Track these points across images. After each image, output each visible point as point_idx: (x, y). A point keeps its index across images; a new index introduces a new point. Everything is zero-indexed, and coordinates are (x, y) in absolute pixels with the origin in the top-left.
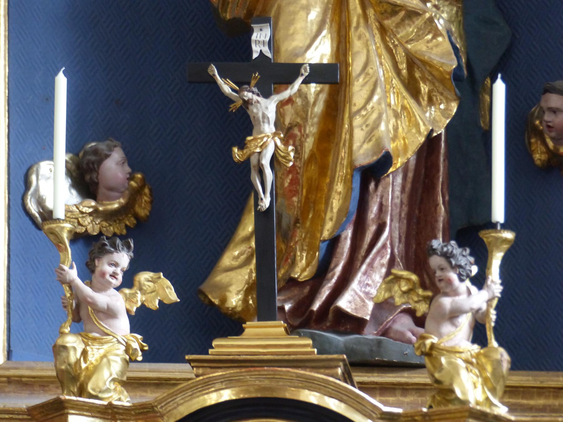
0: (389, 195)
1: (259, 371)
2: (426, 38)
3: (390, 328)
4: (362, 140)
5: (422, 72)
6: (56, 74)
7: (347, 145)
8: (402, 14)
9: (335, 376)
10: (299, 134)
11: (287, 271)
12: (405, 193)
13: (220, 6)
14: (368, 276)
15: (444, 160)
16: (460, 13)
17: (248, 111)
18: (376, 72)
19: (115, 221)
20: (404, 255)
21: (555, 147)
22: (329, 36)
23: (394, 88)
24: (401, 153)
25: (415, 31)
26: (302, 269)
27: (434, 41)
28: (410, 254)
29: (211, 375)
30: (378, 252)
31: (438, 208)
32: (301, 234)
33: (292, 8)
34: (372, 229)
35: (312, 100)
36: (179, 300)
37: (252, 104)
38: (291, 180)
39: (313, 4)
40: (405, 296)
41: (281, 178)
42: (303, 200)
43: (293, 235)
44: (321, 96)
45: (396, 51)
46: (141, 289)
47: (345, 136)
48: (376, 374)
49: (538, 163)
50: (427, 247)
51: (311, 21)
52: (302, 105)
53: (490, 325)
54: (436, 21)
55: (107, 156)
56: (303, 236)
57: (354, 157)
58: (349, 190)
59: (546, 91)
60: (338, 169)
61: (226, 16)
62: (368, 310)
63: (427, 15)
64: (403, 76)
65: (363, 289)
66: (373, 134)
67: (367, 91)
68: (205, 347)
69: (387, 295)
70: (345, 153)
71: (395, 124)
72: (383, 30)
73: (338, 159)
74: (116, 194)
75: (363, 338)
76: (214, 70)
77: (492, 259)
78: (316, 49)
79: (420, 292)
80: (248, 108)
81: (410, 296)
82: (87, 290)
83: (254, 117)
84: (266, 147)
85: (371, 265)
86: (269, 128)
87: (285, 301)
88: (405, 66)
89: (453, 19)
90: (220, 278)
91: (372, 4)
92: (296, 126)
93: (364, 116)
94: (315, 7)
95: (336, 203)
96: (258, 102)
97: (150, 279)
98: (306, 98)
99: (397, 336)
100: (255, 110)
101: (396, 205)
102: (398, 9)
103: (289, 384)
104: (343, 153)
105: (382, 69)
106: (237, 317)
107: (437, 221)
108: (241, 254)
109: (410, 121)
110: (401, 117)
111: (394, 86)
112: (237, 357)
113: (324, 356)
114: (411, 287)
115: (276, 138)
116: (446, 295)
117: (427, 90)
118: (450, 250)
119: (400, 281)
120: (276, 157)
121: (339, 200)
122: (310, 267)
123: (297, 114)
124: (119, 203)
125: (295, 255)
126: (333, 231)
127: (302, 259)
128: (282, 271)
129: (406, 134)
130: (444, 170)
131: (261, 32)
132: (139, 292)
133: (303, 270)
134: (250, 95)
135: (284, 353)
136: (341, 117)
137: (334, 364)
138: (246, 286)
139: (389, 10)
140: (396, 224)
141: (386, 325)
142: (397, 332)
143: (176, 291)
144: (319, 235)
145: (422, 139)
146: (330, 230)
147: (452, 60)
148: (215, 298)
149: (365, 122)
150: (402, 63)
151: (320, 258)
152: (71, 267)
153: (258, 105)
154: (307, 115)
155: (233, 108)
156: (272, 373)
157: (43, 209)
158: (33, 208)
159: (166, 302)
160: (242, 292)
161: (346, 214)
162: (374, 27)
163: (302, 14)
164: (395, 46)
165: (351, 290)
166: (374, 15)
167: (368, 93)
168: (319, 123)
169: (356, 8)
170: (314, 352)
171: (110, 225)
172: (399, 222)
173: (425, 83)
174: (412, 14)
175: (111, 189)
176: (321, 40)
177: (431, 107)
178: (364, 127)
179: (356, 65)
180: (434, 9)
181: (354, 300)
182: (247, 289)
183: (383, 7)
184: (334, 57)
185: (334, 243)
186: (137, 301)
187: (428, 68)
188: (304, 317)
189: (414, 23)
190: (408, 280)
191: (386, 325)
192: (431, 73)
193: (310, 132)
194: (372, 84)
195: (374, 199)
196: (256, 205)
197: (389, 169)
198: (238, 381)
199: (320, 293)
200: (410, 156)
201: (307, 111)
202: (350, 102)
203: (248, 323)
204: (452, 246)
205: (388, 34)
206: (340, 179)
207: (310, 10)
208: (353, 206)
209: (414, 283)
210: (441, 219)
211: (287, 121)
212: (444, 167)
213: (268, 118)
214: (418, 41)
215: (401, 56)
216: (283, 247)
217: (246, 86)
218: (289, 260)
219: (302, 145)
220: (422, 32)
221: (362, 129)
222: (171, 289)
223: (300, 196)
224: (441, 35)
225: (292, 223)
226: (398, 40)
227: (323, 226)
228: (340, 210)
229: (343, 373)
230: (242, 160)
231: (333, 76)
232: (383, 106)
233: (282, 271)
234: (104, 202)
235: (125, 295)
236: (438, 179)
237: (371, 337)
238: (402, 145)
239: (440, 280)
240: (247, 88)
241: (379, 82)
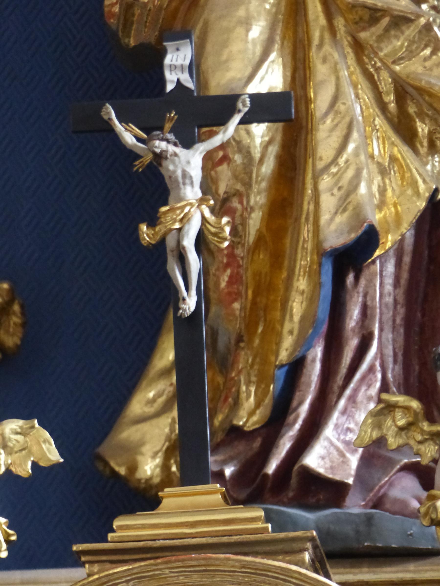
0: (375, 290)
1: (183, 561)
2: (422, 54)
3: (385, 495)
4: (333, 211)
5: (418, 105)
7: (311, 219)
8: (386, 21)
9: (301, 564)
10: (239, 207)
11: (227, 416)
12: (400, 287)
13: (121, 27)
14: (349, 416)
17: (160, 169)
18: (350, 109)
20: (401, 382)
22: (280, 60)
23: (377, 130)
24: (392, 226)
25: (406, 44)
26: (250, 413)
27: (434, 57)
28: (412, 380)
29: (111, 572)
30: (363, 378)
32: (246, 358)
33: (225, 24)
34: (352, 343)
35: (257, 155)
36: (62, 460)
37: (166, 158)
38: (230, 277)
39: (255, 15)
40: (403, 433)
41: (214, 275)
42: (249, 306)
43: (235, 362)
44: (270, 148)
45: (378, 77)
47: (308, 206)
48: (365, 569)
50: (433, 355)
51: (253, 40)
52: (244, 164)
56: (250, 360)
57: (321, 237)
58: (316, 286)
60: (299, 256)
61: (129, 41)
62: (350, 468)
63: (423, 21)
64: (390, 113)
65: (342, 437)
67: (338, 137)
68: (102, 530)
69: (375, 435)
70: (308, 231)
71: (382, 184)
72: (358, 47)
73: (298, 241)
75: (345, 514)
78: (261, 81)
79: (426, 426)
80: (161, 165)
81: (410, 433)
83: (170, 177)
84: (189, 220)
85: (352, 399)
86: (192, 193)
87: (225, 462)
88: (392, 97)
90: (127, 434)
91: (340, 9)
92: (234, 195)
93: (334, 175)
94: (259, 20)
96: (176, 155)
97: (19, 430)
98: (249, 153)
100: (171, 167)
101: (387, 305)
102: (379, 14)
103: (229, 579)
104: (306, 232)
105: (358, 103)
109: (403, 178)
111: (378, 127)
112: (150, 543)
113: (282, 535)
114: (411, 419)
115: (204, 207)
117: (426, 131)
119: (394, 411)
120: (203, 233)
121: (302, 303)
122: (261, 408)
123: (236, 177)
125: (238, 391)
126: (294, 350)
127: (249, 396)
128: (220, 417)
129: (398, 198)
131: (179, 53)
133: (252, 414)
134: (163, 145)
135: (221, 533)
136: (301, 178)
137: (296, 546)
138: (167, 444)
139: (366, 17)
140: (389, 336)
141: (379, 491)
142: (396, 501)
143: (58, 447)
144: (273, 358)
145: (422, 204)
146: (290, 349)
148: (120, 465)
149: (336, 184)
150: (388, 94)
151: (277, 393)
153: (176, 158)
154: (250, 178)
155: (138, 166)
156: (203, 562)
159: (42, 464)
160: (160, 454)
161: (313, 322)
162: (346, 43)
163: (240, 30)
164: (377, 70)
165: (324, 439)
166: (345, 26)
167: (340, 140)
168: (269, 189)
169: (318, 17)
170: (267, 528)
172: (393, 332)
173: (423, 121)
174: (400, 21)
176: (269, 67)
177: (433, 157)
178: (335, 191)
179: (321, 100)
180: (432, 12)
181: (329, 454)
182: (168, 449)
183: (357, 13)
185: (297, 366)
187: (427, 98)
188: (254, 486)
189: (403, 33)
190: (407, 409)
191: (379, 491)
192: (431, 106)
193: (256, 203)
194: (345, 126)
195: (354, 299)
197: (374, 251)
198: (152, 577)
199: (277, 447)
200: (405, 231)
201: (251, 173)
202: (314, 155)
203: (166, 490)
205: (366, 52)
206: (302, 270)
207: (251, 25)
208: (323, 310)
209: (416, 414)
211: (222, 189)
213: (191, 178)
214: (410, 60)
215: (385, 82)
216: (220, 379)
217: (158, 132)
218: (230, 400)
219: (244, 223)
220: (415, 46)
221: (332, 194)
222: (50, 444)
223: (243, 300)
225: (233, 341)
226: (381, 60)
227: (278, 344)
228: (303, 319)
229: (313, 560)
230: (153, 242)
231: (286, 112)
232: (362, 157)
233: (220, 417)
237: (356, 511)
238: (393, 214)
240: (159, 135)
241: (355, 123)
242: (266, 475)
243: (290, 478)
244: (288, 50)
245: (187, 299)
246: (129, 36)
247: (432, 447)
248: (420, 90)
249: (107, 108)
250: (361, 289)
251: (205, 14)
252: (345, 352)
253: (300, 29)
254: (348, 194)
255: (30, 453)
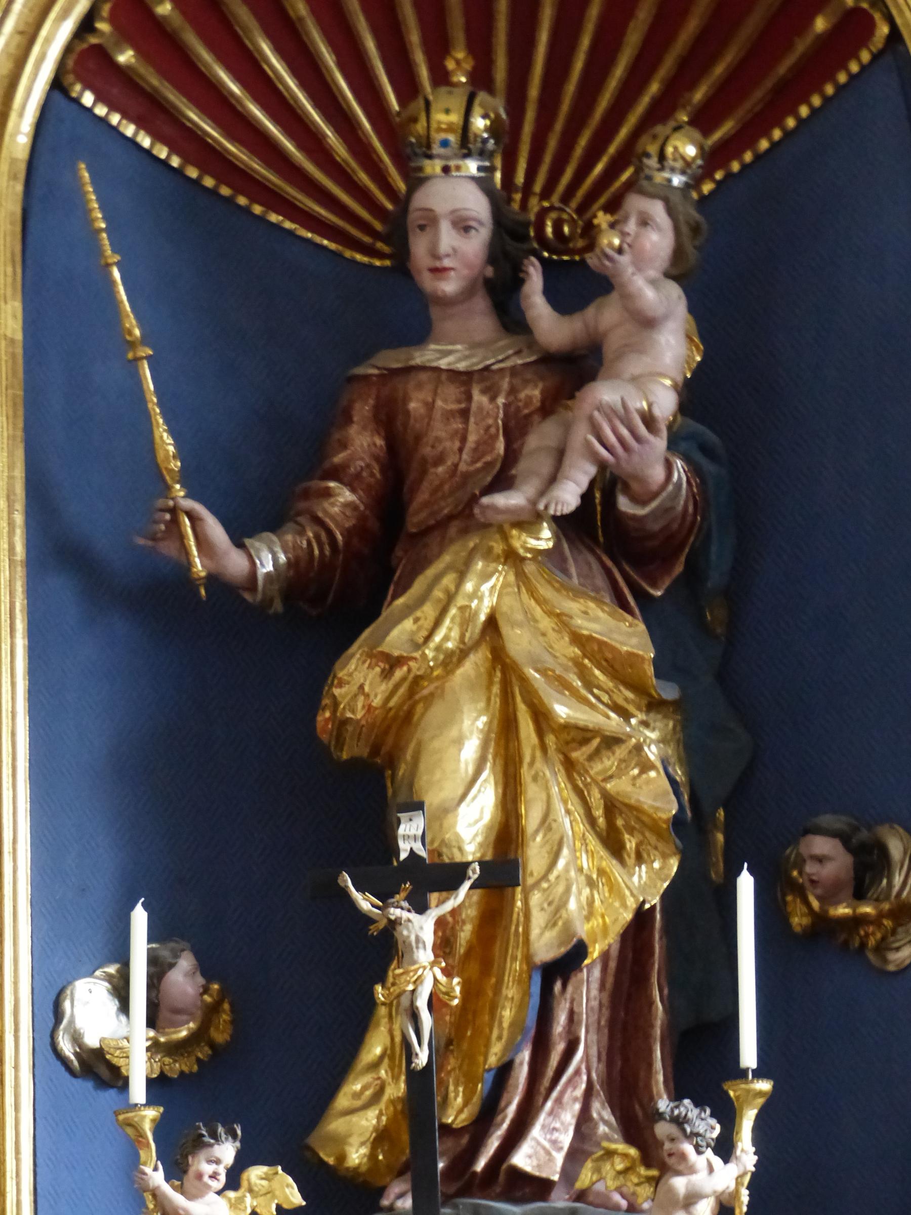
4: (543, 925)
6: (133, 907)
8: (596, 742)
13: (333, 743)
14: (555, 1116)
15: (661, 938)
16: (678, 728)
19: (182, 1055)
21: (821, 907)
27: (644, 776)
31: (654, 1008)
33: (436, 744)
36: (304, 1203)
37: (401, 924)
39: (468, 734)
40: (621, 1178)
46: (251, 1191)
49: (798, 929)
53: (741, 1211)
54: (646, 749)
55: (171, 966)
57: (532, 951)
58: (526, 994)
59: (807, 832)
65: (548, 1136)
66: (558, 916)
72: (570, 766)
74: (185, 1017)
75: (550, 1208)
76: (347, 880)
77: (741, 1118)
79: (643, 1171)
80: (395, 929)
82: (178, 1199)
83: (404, 942)
84: (422, 982)
85: (559, 1101)
86: (425, 956)
89: (669, 737)
90: (335, 1125)
93: (545, 890)
95: (507, 1014)
96: (409, 920)
99: (597, 1201)
100: (405, 933)
101: (592, 1008)
106: (361, 1179)
107: (652, 1026)
108: (364, 1088)
110: (598, 886)
114: (628, 1165)
116: (679, 1173)
118: (684, 1114)
120: (439, 1000)
124: (189, 1029)
126: (503, 1055)
130: (660, 953)
131: (411, 823)
132: (248, 1195)
133: (460, 1111)
134: (398, 912)
138: (374, 1135)
140: (593, 1037)
142: (598, 1194)
144: (481, 1059)
145: (628, 916)
146: (499, 1054)
147: (669, 802)
148: (329, 1156)
149: (546, 899)
150: (597, 809)
151: (486, 1091)
152: (156, 1169)
153: (410, 924)
155: (374, 930)
157: (80, 1048)
158: (67, 1048)
159: (285, 1206)
171: (175, 1061)
175: (177, 1011)
176: (481, 786)
177: (640, 867)
182: (375, 1139)
184: (500, 807)
185: (505, 1070)
186: (246, 1207)
187: (635, 813)
189: (614, 753)
190: (625, 1156)
193: (467, 916)
196: (409, 1061)
199: (486, 1146)
204: (686, 1107)
207: (463, 744)
209: (633, 1160)
210: (658, 1023)
212: (661, 948)
213: (424, 943)
215: (595, 799)
219: (455, 935)
222: (293, 1188)
224: (653, 767)
226: (591, 777)
227: (487, 1046)
228: (512, 1025)
231: (502, 869)
232: (573, 873)
234: (167, 1030)
235: (229, 1200)
236: (653, 964)
239: (670, 1155)
241: (565, 839)
242: (475, 1173)
243: (498, 1175)
244: (499, 768)
245: (420, 1055)
246: (342, 750)
247: (647, 1189)
248: (630, 807)
249: (343, 876)
250: (568, 995)
251: (418, 735)
252: (552, 1056)
253: (511, 745)
254: (557, 910)
255: (274, 1197)
